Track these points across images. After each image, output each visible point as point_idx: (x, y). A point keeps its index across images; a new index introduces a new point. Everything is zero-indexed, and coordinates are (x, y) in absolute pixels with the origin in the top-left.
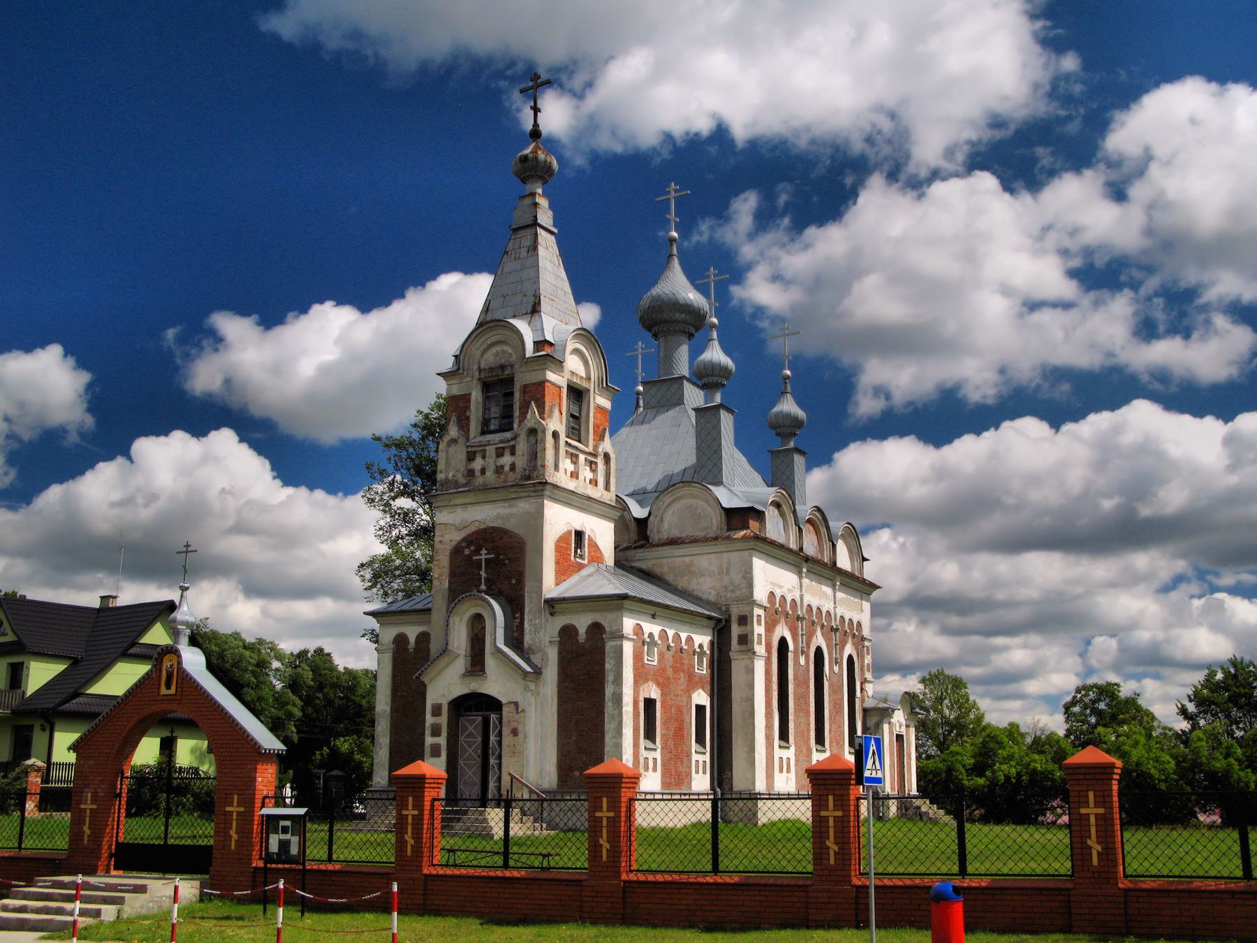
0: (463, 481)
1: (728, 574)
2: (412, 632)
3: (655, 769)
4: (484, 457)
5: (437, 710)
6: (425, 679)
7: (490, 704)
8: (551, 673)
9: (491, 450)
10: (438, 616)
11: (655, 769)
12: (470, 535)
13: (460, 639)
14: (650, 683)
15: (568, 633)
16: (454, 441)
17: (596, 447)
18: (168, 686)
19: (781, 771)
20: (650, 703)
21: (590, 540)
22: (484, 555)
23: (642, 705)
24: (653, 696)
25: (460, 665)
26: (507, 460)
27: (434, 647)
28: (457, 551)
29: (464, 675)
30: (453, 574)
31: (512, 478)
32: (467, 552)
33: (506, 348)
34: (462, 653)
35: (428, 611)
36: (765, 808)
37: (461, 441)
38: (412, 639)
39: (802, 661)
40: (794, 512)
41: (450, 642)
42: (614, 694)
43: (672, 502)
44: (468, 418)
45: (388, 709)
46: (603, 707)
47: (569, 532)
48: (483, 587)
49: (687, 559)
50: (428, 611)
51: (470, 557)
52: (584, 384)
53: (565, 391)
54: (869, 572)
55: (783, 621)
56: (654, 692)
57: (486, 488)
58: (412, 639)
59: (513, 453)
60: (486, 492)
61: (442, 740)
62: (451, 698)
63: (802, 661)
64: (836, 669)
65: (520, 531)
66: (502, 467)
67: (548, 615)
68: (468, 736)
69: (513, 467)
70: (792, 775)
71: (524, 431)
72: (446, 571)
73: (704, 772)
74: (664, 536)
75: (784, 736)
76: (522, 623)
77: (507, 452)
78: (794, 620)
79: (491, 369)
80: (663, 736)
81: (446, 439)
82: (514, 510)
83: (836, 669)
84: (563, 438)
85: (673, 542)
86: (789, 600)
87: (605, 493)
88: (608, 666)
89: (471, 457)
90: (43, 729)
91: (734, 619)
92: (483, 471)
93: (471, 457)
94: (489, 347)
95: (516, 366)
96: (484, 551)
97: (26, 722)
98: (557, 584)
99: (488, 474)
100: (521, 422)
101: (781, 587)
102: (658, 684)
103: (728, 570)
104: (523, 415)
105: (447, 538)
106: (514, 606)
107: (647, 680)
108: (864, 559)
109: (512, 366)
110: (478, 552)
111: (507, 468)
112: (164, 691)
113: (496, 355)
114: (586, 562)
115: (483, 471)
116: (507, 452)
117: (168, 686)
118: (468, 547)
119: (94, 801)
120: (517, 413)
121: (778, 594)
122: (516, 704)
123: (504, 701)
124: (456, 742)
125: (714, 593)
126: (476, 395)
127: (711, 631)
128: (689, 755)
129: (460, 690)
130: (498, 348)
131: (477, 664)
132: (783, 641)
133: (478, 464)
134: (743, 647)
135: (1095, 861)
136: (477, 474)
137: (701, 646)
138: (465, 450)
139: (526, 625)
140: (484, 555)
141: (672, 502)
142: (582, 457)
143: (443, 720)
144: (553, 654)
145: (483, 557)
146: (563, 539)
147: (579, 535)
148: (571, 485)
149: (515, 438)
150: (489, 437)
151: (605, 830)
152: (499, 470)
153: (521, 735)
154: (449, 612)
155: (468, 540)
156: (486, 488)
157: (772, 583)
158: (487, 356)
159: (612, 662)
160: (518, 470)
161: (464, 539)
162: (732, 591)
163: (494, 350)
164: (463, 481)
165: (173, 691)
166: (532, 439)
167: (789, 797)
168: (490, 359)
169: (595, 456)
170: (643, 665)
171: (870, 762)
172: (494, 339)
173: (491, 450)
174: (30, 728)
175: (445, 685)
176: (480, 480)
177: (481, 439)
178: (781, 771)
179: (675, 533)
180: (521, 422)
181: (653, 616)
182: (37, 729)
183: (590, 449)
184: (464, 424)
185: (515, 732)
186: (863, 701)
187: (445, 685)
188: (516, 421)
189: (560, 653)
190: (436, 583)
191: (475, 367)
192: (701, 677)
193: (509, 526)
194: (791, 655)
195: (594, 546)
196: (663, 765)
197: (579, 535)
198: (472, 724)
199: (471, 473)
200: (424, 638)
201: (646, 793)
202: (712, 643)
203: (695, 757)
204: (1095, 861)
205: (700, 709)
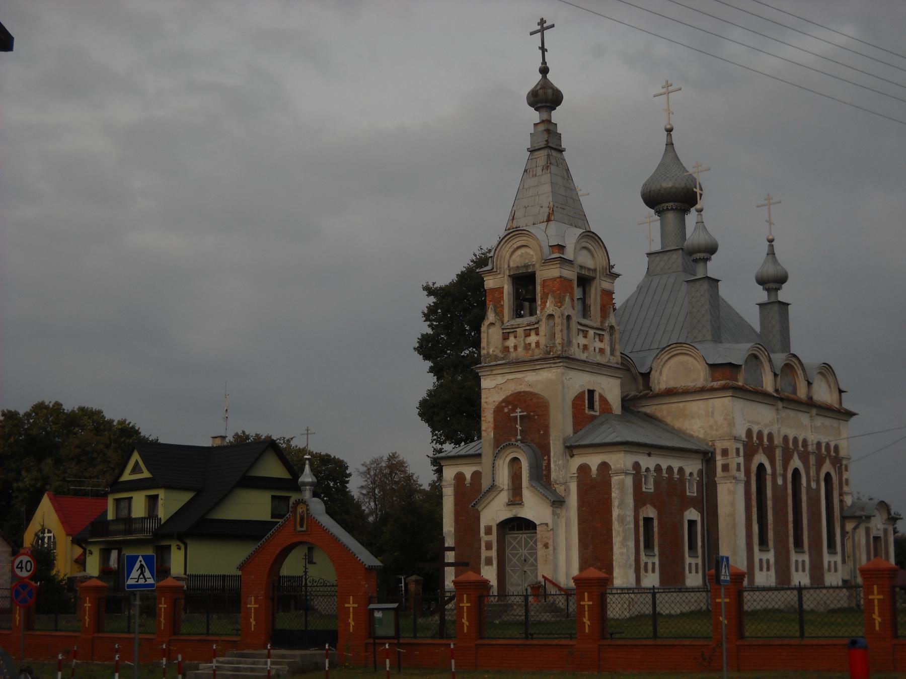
0: (500, 355)
1: (712, 416)
2: (468, 471)
3: (653, 571)
4: (515, 337)
5: (488, 531)
6: (479, 509)
7: (527, 525)
8: (573, 500)
9: (520, 331)
10: (487, 459)
11: (653, 571)
12: (507, 397)
13: (503, 477)
14: (648, 506)
15: (584, 469)
16: (492, 324)
17: (602, 322)
18: (302, 526)
19: (761, 569)
20: (648, 521)
21: (601, 396)
22: (518, 413)
23: (641, 523)
24: (651, 516)
25: (503, 497)
26: (533, 339)
27: (485, 483)
28: (498, 410)
29: (508, 505)
30: (496, 428)
31: (538, 354)
32: (506, 410)
33: (528, 250)
34: (506, 487)
35: (479, 456)
36: (661, 599)
37: (498, 325)
38: (468, 476)
39: (780, 481)
40: (770, 361)
41: (497, 479)
42: (619, 515)
43: (669, 359)
44: (502, 306)
45: (453, 530)
46: (611, 526)
47: (584, 392)
48: (519, 437)
49: (681, 405)
50: (479, 456)
51: (509, 413)
52: (591, 274)
53: (576, 282)
54: (847, 405)
55: (761, 450)
56: (650, 512)
57: (518, 363)
58: (468, 476)
59: (537, 334)
60: (519, 364)
61: (494, 553)
62: (499, 521)
63: (780, 481)
64: (813, 485)
65: (545, 394)
66: (530, 344)
67: (569, 457)
68: (512, 549)
69: (538, 344)
70: (772, 573)
71: (545, 317)
72: (492, 425)
73: (697, 572)
74: (663, 386)
75: (763, 542)
76: (549, 460)
77: (533, 333)
78: (770, 452)
79: (518, 267)
80: (660, 546)
81: (486, 323)
82: (540, 378)
83: (813, 485)
84: (574, 319)
85: (671, 393)
86: (766, 433)
87: (612, 358)
88: (613, 495)
89: (506, 337)
90: (179, 548)
91: (718, 452)
92: (515, 348)
93: (506, 337)
94: (519, 248)
95: (537, 266)
96: (518, 410)
97: (165, 543)
98: (575, 432)
99: (519, 350)
100: (542, 309)
101: (758, 424)
102: (654, 506)
103: (713, 413)
104: (544, 303)
105: (491, 400)
106: (541, 452)
107: (644, 505)
108: (841, 392)
109: (534, 265)
110: (514, 410)
111: (533, 345)
112: (299, 529)
113: (521, 256)
114: (598, 414)
115: (515, 348)
116: (533, 333)
117: (302, 526)
118: (507, 406)
119: (256, 602)
120: (539, 302)
121: (755, 429)
122: (547, 524)
123: (537, 523)
124: (504, 553)
125: (702, 431)
126: (507, 288)
127: (700, 462)
128: (683, 559)
129: (506, 514)
130: (523, 250)
131: (516, 498)
132: (761, 467)
133: (511, 342)
134: (725, 474)
135: (877, 628)
136: (512, 350)
137: (691, 474)
138: (501, 332)
139: (552, 466)
140: (518, 413)
141: (669, 359)
142: (591, 332)
143: (493, 538)
144: (573, 487)
145: (518, 414)
146: (579, 398)
147: (591, 393)
148: (583, 356)
149: (537, 323)
150: (519, 320)
151: (586, 613)
152: (527, 347)
153: (551, 548)
154: (496, 457)
155: (507, 401)
156: (518, 363)
157: (749, 422)
158: (514, 257)
159: (617, 492)
160: (541, 347)
161: (504, 401)
162: (717, 430)
163: (519, 252)
164: (500, 355)
165: (304, 529)
166: (551, 322)
167: (769, 589)
168: (516, 260)
169: (603, 330)
170: (642, 493)
171: (723, 571)
172: (519, 244)
173: (520, 331)
174: (169, 548)
175: (494, 512)
176: (513, 355)
177: (513, 322)
178: (761, 569)
179: (672, 384)
180: (542, 309)
181: (649, 455)
182: (174, 549)
183: (597, 324)
184: (499, 313)
185: (546, 546)
186: (842, 509)
187: (494, 512)
188: (539, 308)
189: (578, 486)
190: (484, 434)
191: (506, 266)
192: (692, 498)
193: (537, 390)
194: (769, 479)
195: (603, 399)
196: (684, 568)
197: (591, 393)
198: (518, 538)
199: (506, 349)
200: (477, 475)
201: (617, 589)
202: (700, 472)
203: (688, 560)
204: (877, 628)
205: (692, 523)
